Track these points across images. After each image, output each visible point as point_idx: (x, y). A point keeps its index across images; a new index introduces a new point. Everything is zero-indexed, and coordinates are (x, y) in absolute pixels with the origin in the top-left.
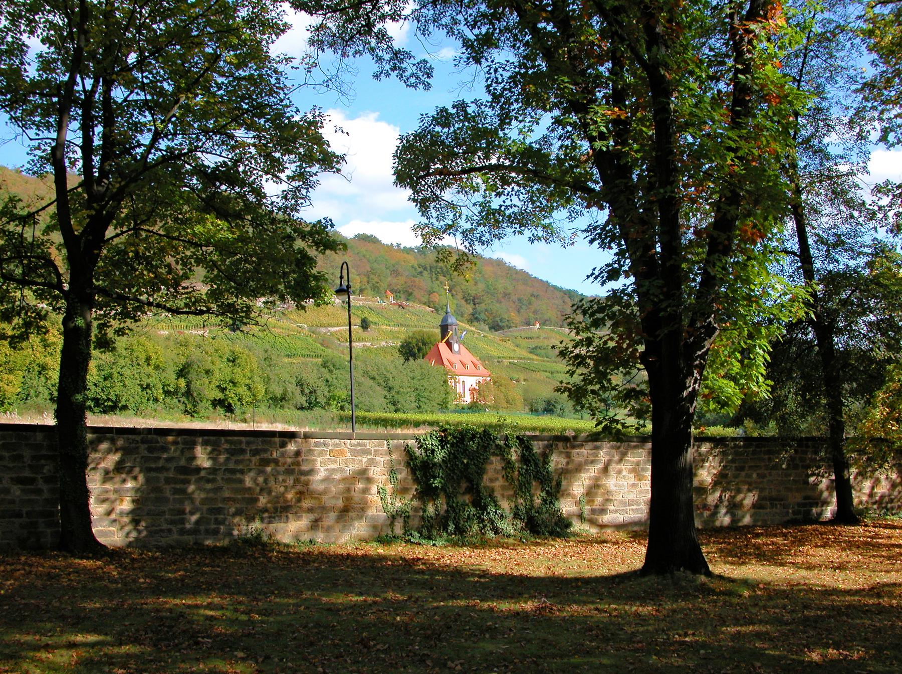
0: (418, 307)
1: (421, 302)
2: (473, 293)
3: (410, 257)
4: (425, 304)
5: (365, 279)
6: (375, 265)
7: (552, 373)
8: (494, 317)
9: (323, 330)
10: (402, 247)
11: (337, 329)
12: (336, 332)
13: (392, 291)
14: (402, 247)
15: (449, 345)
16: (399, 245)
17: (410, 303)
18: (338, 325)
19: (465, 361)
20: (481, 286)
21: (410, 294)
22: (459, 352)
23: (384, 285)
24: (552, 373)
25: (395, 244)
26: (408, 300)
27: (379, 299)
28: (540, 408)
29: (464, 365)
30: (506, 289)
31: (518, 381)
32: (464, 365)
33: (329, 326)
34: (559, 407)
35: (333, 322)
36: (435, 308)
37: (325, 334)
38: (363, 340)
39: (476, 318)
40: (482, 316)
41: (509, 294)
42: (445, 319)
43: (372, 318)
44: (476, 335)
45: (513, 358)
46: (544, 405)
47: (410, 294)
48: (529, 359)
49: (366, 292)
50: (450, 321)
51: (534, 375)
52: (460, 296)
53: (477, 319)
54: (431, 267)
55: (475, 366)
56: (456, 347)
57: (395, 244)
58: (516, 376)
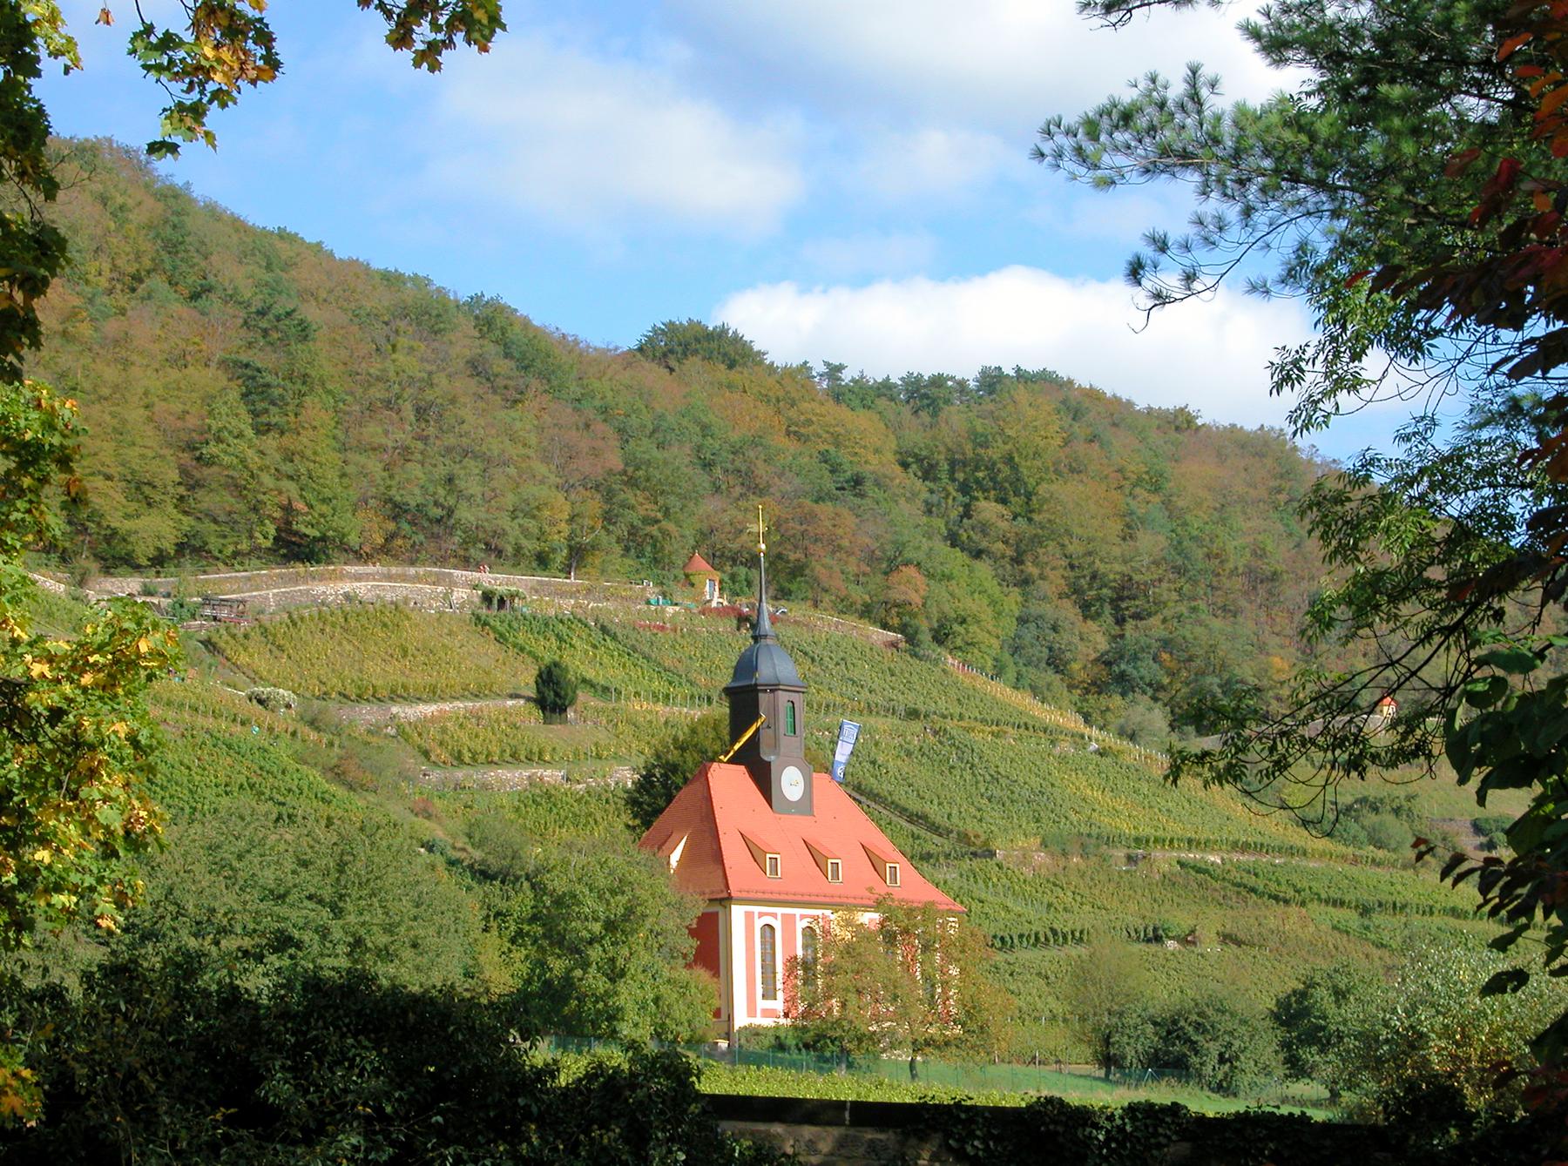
0: (829, 625)
1: (845, 606)
2: (1113, 571)
3: (861, 422)
4: (866, 612)
5: (594, 506)
6: (645, 448)
7: (1365, 911)
8: (1201, 673)
9: (367, 714)
10: (847, 376)
11: (429, 709)
12: (421, 725)
13: (717, 558)
14: (847, 376)
15: (763, 778)
16: (834, 371)
17: (795, 610)
18: (434, 695)
19: (824, 842)
20: (1151, 543)
21: (797, 571)
22: (806, 805)
23: (681, 534)
24: (1365, 911)
25: (818, 368)
26: (783, 594)
27: (651, 591)
28: (1131, 1050)
29: (818, 858)
30: (1259, 553)
31: (1189, 939)
32: (818, 858)
33: (395, 696)
34: (1214, 1049)
35: (419, 679)
36: (903, 629)
37: (374, 731)
38: (535, 757)
39: (1122, 678)
40: (1147, 669)
41: (1274, 577)
42: (746, 666)
43: (578, 663)
44: (1066, 747)
45: (1206, 845)
46: (1150, 1038)
47: (797, 571)
48: (1291, 851)
49: (597, 560)
50: (764, 673)
51: (1273, 916)
52: (1054, 581)
53: (1124, 684)
54: (953, 464)
55: (876, 863)
56: (791, 783)
57: (818, 368)
58: (1181, 920)
